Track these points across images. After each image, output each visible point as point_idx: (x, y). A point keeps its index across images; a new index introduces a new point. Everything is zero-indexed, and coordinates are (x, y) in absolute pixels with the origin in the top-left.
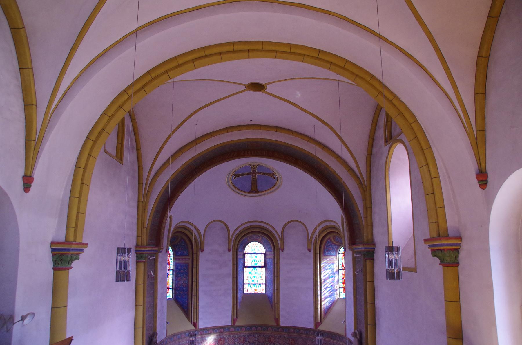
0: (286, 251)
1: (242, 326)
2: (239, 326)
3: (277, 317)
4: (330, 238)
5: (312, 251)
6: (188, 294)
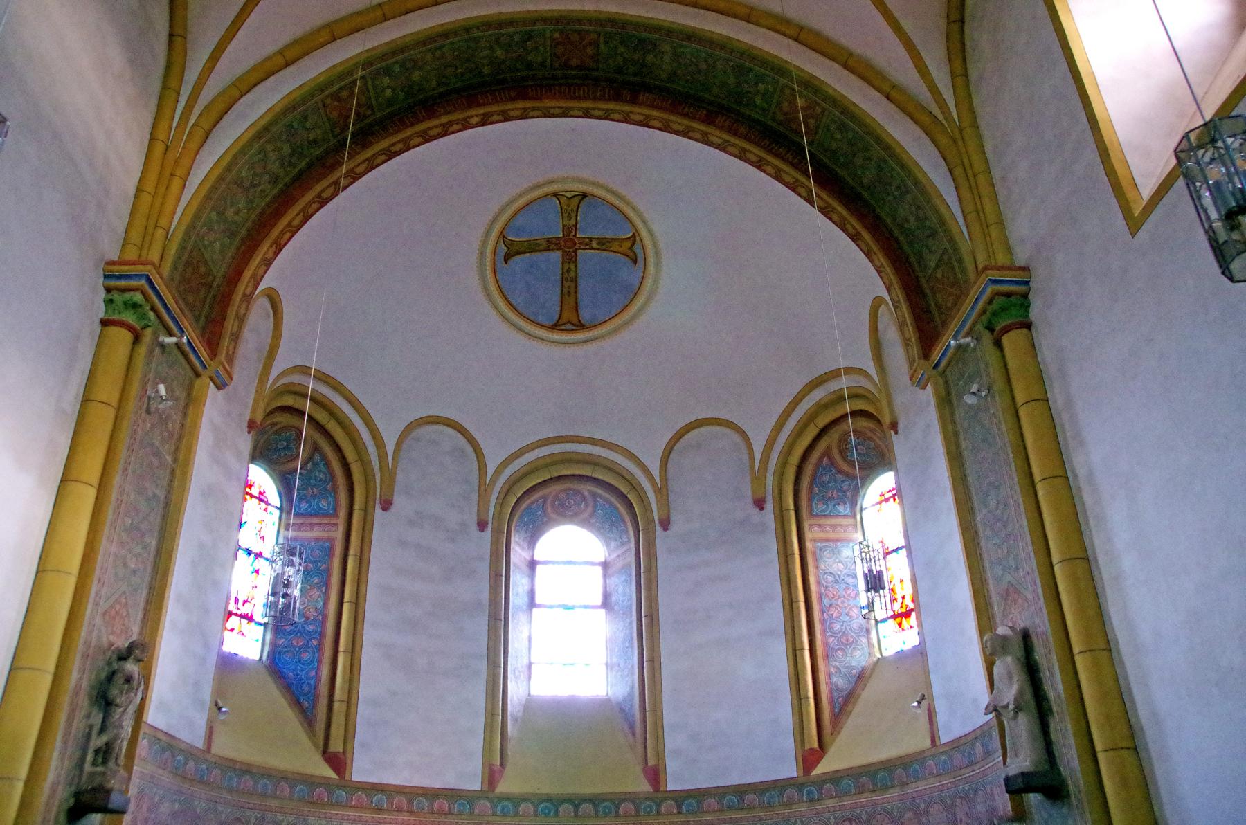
0: (677, 526)
1: (524, 799)
2: (508, 797)
3: (651, 762)
4: (827, 453)
5: (769, 506)
6: (320, 648)
